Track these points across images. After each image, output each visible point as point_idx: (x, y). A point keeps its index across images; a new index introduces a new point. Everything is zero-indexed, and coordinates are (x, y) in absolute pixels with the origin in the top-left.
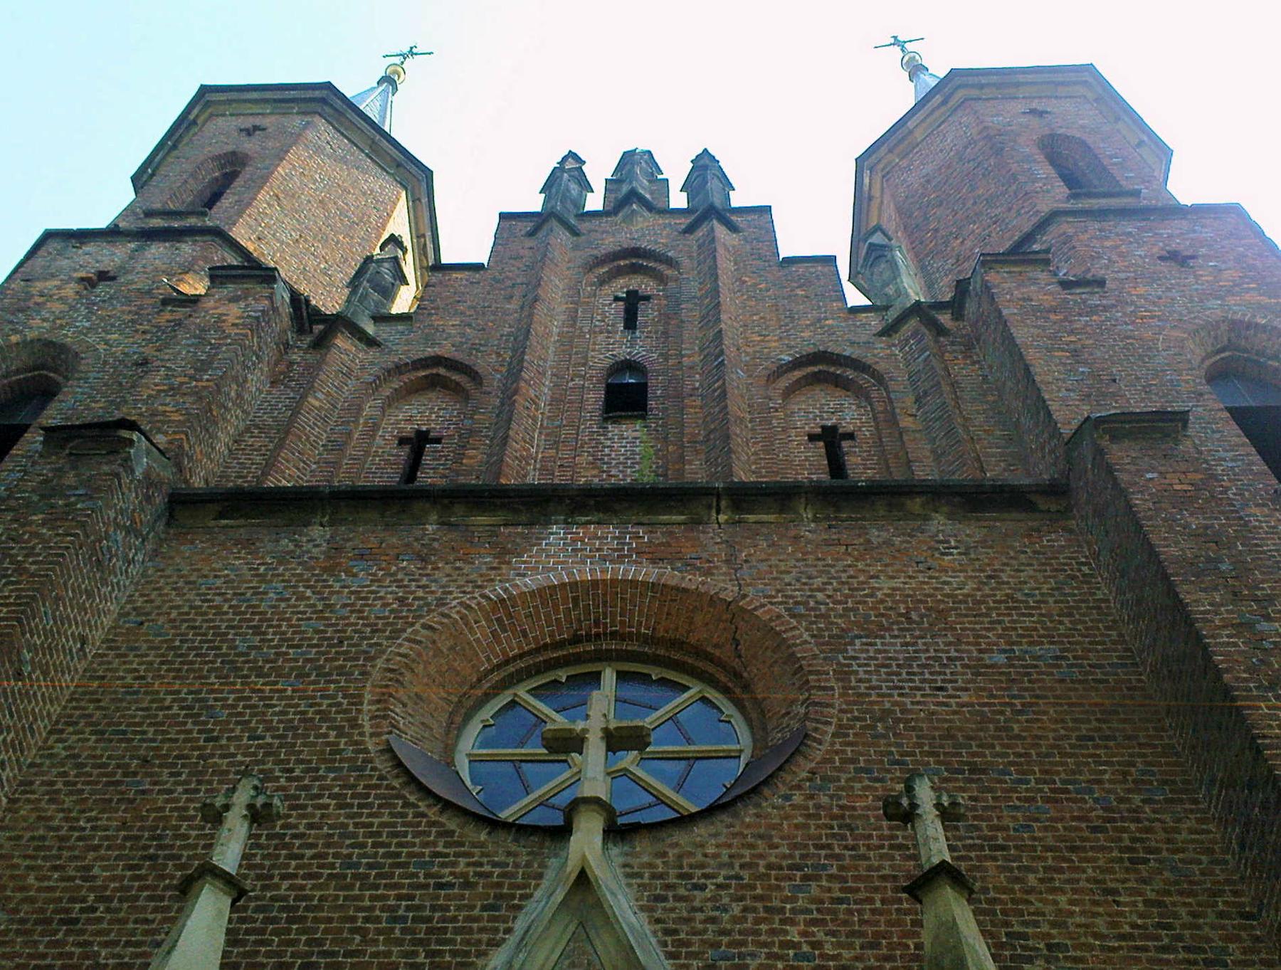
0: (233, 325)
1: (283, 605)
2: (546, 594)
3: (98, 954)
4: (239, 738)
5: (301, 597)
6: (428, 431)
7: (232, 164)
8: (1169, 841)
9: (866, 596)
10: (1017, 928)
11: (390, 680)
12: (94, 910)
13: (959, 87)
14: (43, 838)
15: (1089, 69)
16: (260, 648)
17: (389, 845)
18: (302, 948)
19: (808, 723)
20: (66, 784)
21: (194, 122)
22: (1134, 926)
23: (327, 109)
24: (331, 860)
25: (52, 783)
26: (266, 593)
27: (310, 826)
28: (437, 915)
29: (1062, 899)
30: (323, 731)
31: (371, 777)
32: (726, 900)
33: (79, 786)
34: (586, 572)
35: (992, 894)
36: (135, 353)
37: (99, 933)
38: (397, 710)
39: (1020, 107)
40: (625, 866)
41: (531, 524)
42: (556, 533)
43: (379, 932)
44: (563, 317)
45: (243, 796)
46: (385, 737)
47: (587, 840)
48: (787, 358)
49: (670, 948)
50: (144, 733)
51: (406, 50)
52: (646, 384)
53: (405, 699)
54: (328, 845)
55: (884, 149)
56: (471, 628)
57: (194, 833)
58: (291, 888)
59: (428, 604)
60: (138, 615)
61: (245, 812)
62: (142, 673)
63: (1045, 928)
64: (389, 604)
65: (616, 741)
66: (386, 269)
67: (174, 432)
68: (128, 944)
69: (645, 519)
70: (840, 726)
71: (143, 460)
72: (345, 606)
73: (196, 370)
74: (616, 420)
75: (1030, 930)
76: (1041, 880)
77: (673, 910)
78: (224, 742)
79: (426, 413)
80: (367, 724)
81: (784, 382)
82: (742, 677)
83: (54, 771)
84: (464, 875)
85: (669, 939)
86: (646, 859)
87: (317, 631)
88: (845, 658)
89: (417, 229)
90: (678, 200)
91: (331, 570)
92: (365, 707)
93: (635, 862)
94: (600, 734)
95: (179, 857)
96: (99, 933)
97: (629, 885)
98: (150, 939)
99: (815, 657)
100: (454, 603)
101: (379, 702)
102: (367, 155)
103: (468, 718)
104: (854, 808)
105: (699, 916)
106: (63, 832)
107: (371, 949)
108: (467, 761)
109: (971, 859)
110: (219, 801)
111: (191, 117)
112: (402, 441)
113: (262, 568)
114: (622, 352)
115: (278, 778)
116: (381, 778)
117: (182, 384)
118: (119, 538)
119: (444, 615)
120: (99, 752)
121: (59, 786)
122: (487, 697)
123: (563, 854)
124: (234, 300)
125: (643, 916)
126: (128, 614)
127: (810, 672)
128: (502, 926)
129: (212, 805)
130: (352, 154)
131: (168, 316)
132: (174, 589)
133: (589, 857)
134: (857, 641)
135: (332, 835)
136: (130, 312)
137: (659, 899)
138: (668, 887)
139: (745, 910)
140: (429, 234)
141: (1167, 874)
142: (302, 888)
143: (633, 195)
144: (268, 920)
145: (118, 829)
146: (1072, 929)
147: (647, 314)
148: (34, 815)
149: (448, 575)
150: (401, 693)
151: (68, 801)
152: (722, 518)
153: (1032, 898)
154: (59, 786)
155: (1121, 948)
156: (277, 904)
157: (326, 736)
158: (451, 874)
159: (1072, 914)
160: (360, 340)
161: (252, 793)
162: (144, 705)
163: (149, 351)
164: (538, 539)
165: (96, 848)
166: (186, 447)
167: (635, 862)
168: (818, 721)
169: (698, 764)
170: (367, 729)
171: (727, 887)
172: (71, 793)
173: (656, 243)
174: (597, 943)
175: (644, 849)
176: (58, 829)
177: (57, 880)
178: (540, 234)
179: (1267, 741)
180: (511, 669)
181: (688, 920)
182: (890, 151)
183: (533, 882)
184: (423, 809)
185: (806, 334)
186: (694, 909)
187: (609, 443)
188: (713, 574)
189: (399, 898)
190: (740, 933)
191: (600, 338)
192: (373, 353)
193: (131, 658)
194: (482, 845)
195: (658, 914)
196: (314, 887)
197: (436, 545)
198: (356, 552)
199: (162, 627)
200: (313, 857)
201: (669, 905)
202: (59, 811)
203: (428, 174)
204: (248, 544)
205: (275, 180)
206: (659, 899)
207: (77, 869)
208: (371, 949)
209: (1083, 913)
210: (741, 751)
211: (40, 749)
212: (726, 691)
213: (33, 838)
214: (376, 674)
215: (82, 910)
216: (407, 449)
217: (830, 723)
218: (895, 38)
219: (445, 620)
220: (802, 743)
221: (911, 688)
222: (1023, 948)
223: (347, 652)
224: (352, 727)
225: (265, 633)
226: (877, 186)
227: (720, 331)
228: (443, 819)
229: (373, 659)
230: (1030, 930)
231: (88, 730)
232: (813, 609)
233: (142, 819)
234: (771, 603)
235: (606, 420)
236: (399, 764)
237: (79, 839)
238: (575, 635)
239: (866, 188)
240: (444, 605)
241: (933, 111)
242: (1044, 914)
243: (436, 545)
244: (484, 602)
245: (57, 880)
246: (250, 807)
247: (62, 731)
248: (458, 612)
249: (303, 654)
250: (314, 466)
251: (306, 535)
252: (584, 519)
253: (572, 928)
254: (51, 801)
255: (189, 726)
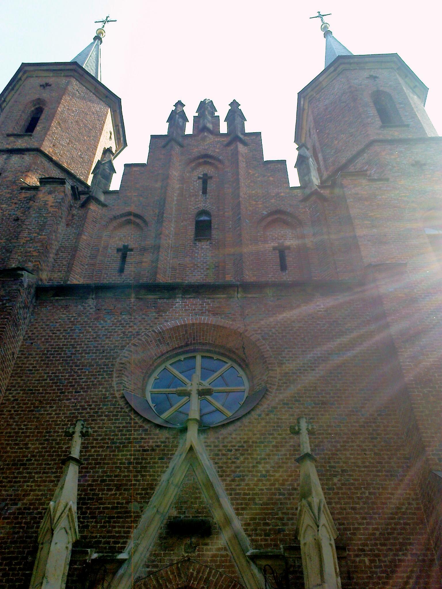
0: (51, 206)
1: (82, 335)
2: (176, 329)
3: (34, 477)
4: (72, 392)
5: (88, 332)
6: (128, 245)
7: (39, 104)
8: (385, 430)
9: (290, 330)
10: (332, 464)
11: (122, 367)
12: (31, 460)
13: (341, 64)
14: (10, 433)
15: (395, 55)
16: (75, 354)
17: (126, 435)
18: (100, 474)
19: (267, 385)
20: (15, 411)
21: (20, 79)
22: (370, 463)
23: (76, 74)
24: (107, 441)
25: (10, 411)
26: (75, 330)
27: (99, 427)
28: (144, 461)
29: (348, 453)
30: (100, 389)
31: (118, 408)
32: (239, 455)
33: (19, 412)
34: (189, 320)
35: (326, 452)
36: (14, 214)
37: (34, 469)
38: (125, 379)
39: (366, 74)
40: (205, 442)
41: (169, 298)
42: (179, 302)
43: (125, 468)
44: (178, 192)
45: (78, 428)
46: (122, 392)
47: (193, 435)
48: (265, 213)
49: (220, 473)
50: (39, 390)
51: (105, 19)
52: (211, 220)
53: (127, 374)
54: (106, 435)
55: (309, 90)
56: (149, 344)
57: (60, 430)
58: (95, 451)
59: (134, 335)
60: (30, 340)
61: (80, 435)
62: (35, 365)
63: (341, 464)
64: (120, 335)
65: (203, 393)
66: (106, 167)
67: (35, 261)
68: (44, 473)
69: (210, 296)
70: (279, 386)
71: (27, 278)
72: (104, 335)
73: (40, 230)
74: (200, 240)
75: (337, 465)
76: (341, 446)
77: (221, 459)
78: (66, 394)
79: (126, 236)
80: (115, 386)
81: (264, 223)
82: (245, 361)
83: (10, 406)
84: (152, 446)
85: (220, 470)
86: (212, 440)
87: (94, 347)
88: (281, 357)
89: (115, 123)
90: (223, 128)
91: (97, 319)
92: (114, 379)
93: (208, 441)
94: (197, 392)
95: (56, 440)
96: (34, 469)
97: (207, 450)
98: (50, 471)
99: (271, 357)
100: (143, 334)
101: (119, 377)
102: (94, 93)
103: (149, 377)
104: (282, 419)
105: (230, 461)
106: (16, 430)
107: (123, 474)
108: (150, 395)
109: (319, 438)
110: (71, 430)
111: (19, 76)
112: (118, 250)
113: (73, 319)
114: (202, 206)
115: (87, 408)
116: (122, 408)
117: (35, 237)
118: (21, 312)
119: (139, 339)
120: (24, 398)
121: (13, 412)
122: (156, 368)
123: (184, 438)
124: (50, 193)
125: (211, 461)
126: (27, 339)
127: (269, 364)
128: (165, 466)
129: (69, 432)
130: (87, 94)
131: (23, 195)
132: (42, 328)
133: (193, 442)
134: (286, 350)
135: (106, 431)
136: (8, 193)
137: (218, 455)
138: (219, 450)
139: (245, 459)
140: (120, 125)
141: (383, 443)
142: (99, 451)
143: (205, 129)
144: (88, 464)
145: (35, 429)
146: (350, 464)
147: (211, 186)
148: (6, 424)
149: (140, 321)
150: (126, 373)
151: (17, 418)
152: (239, 296)
153: (338, 453)
154: (13, 412)
155: (365, 471)
156: (91, 458)
157: (101, 391)
158: (148, 446)
159: (350, 458)
160: (99, 204)
161: (82, 427)
162: (37, 378)
163: (19, 214)
164: (172, 305)
165: (29, 437)
166: (40, 266)
167: (208, 441)
168: (271, 384)
169: (231, 394)
170: (116, 389)
171: (239, 450)
172: (17, 415)
173: (215, 152)
174: (197, 473)
175: (212, 437)
176: (14, 429)
177: (17, 449)
178: (168, 147)
179: (415, 406)
180: (164, 357)
181: (226, 463)
182: (312, 90)
183: (175, 449)
184: (137, 421)
185: (273, 201)
186: (228, 459)
187: (197, 251)
188: (235, 321)
189: (131, 455)
190: (243, 467)
191: (193, 199)
192: (104, 209)
193: (30, 359)
194: (157, 435)
195: (216, 461)
196: (102, 451)
197: (135, 307)
198: (106, 311)
199: (39, 345)
200: (101, 440)
201: (220, 457)
202: (14, 422)
203: (119, 100)
204: (66, 307)
205: (57, 116)
206: (218, 455)
207: (23, 444)
208: (123, 474)
209: (354, 458)
210: (245, 389)
211: (4, 397)
212: (240, 365)
213: (7, 433)
214: (117, 365)
215: (27, 460)
216: (120, 254)
217: (275, 385)
218: (319, 12)
219: (140, 342)
220: (265, 393)
221: (304, 370)
222: (334, 471)
223: (106, 356)
224: (110, 388)
225: (76, 348)
226: (306, 105)
227: (240, 217)
228: (144, 425)
229: (115, 358)
230: (337, 465)
231: (19, 389)
232: (271, 336)
233: (43, 425)
234: (257, 334)
235: (196, 240)
236: (127, 403)
237: (22, 433)
238: (186, 343)
239: (302, 106)
240: (139, 335)
241: (330, 74)
242: (341, 459)
243: (135, 307)
244: (153, 334)
245: (17, 449)
246: (81, 432)
247: (10, 390)
248: (145, 338)
249: (91, 356)
250: (86, 267)
251: (87, 303)
252: (189, 296)
253: (188, 467)
254: (10, 418)
255: (54, 387)
